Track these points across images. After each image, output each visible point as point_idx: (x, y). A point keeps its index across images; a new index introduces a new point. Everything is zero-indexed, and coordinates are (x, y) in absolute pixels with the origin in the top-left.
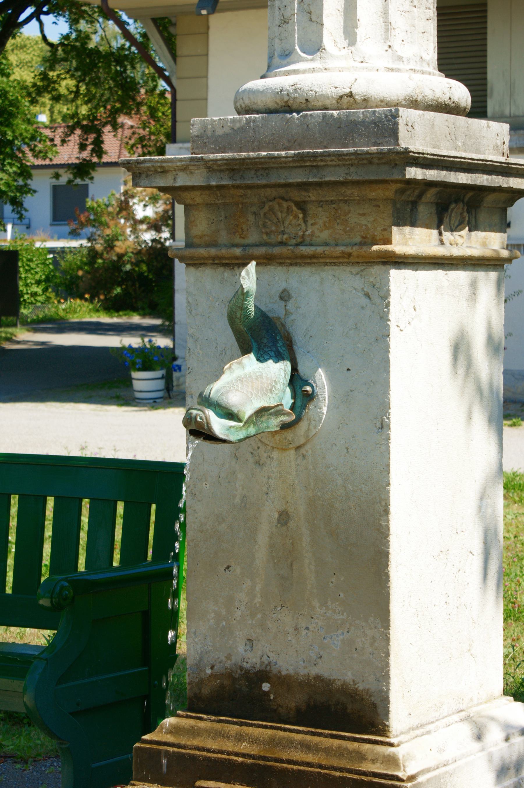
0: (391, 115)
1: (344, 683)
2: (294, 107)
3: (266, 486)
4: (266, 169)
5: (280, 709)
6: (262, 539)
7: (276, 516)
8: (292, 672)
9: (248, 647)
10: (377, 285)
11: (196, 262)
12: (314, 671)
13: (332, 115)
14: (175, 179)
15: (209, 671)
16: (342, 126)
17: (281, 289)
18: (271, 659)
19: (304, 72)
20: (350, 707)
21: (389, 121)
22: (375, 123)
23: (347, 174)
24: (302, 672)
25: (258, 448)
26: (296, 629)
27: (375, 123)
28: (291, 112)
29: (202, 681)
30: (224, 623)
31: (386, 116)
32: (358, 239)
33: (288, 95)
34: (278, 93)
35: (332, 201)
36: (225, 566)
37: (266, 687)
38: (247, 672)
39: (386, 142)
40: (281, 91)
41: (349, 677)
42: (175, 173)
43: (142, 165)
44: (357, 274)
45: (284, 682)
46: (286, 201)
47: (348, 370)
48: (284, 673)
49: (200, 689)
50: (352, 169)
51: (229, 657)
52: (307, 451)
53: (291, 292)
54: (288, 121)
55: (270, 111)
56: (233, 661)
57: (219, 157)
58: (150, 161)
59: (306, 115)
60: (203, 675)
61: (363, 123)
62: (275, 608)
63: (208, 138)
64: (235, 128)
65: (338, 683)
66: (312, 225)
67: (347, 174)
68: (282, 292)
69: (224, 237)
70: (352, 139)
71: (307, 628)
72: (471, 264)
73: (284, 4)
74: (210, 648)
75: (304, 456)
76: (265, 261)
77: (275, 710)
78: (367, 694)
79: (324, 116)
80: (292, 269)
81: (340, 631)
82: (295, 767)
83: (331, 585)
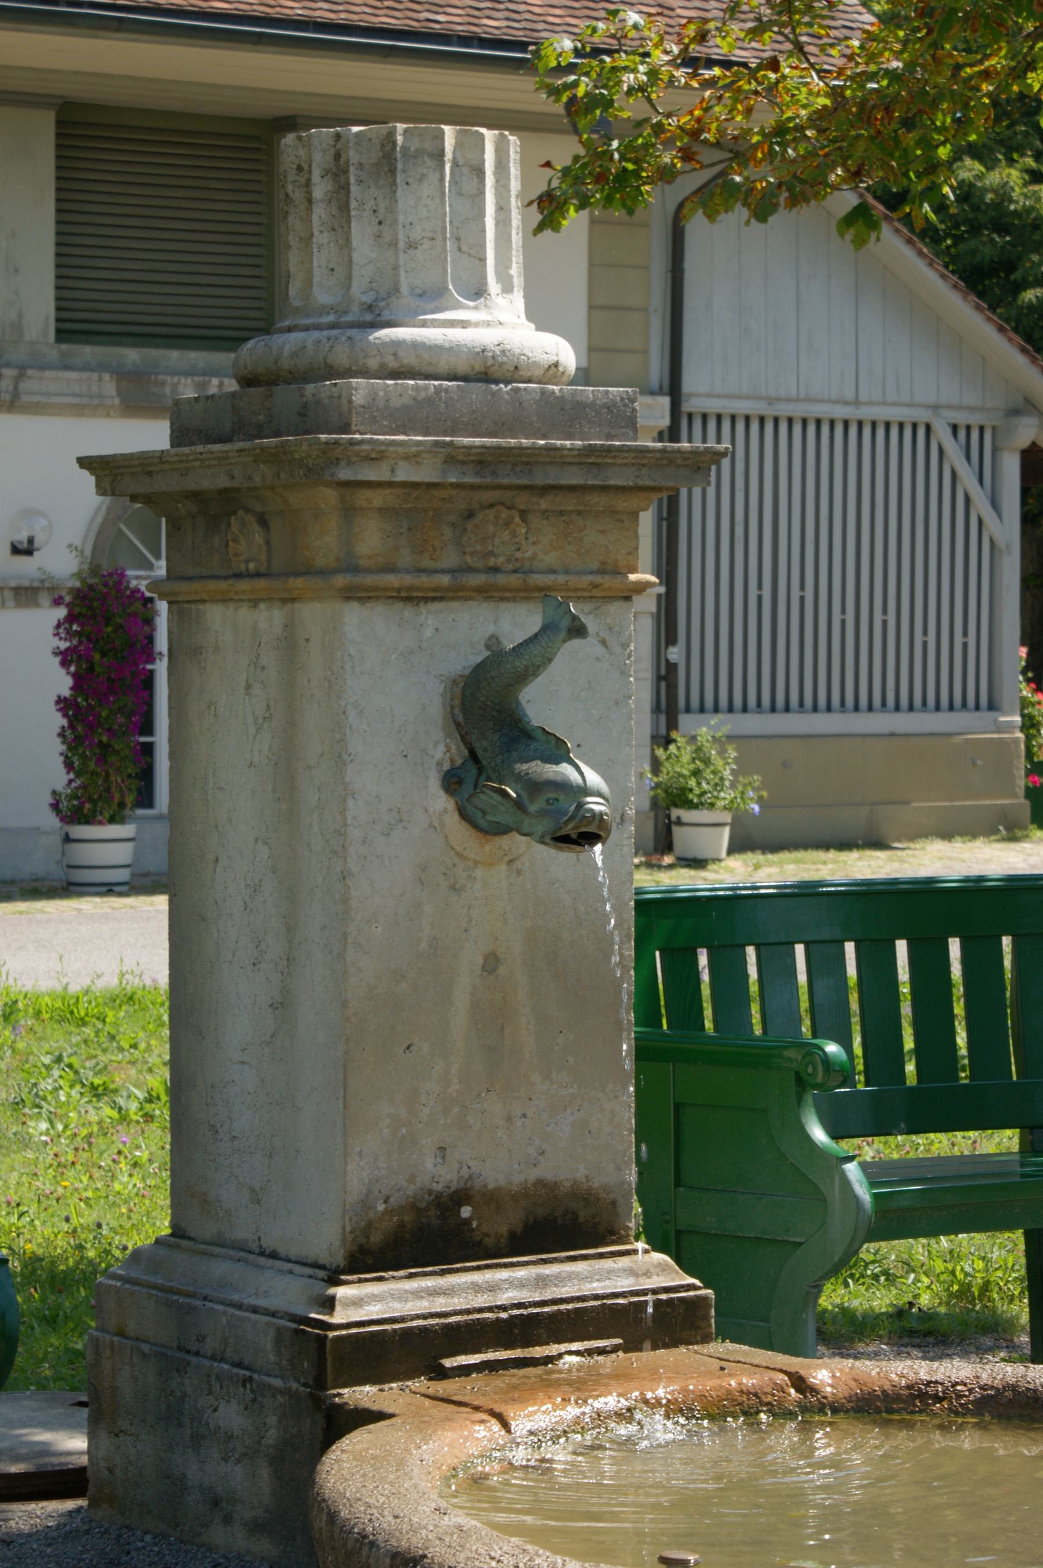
0: (628, 399)
1: (575, 1182)
2: (497, 375)
3: (466, 919)
4: (528, 463)
5: (486, 1239)
6: (461, 998)
7: (480, 961)
8: (502, 1182)
9: (439, 1160)
10: (616, 629)
11: (371, 594)
12: (533, 1175)
13: (553, 392)
14: (393, 471)
15: (381, 1207)
16: (567, 407)
17: (488, 635)
18: (473, 1169)
19: (477, 325)
20: (581, 1214)
21: (626, 406)
22: (608, 408)
23: (637, 477)
24: (517, 1179)
25: (454, 865)
26: (509, 1119)
27: (608, 408)
28: (497, 382)
29: (370, 1224)
30: (404, 1131)
31: (622, 399)
32: (595, 566)
33: (493, 357)
34: (478, 353)
35: (561, 512)
36: (406, 1045)
37: (466, 1212)
38: (439, 1196)
39: (623, 434)
40: (483, 351)
41: (580, 1173)
42: (392, 462)
43: (357, 448)
44: (590, 613)
45: (492, 1199)
46: (509, 508)
47: (579, 745)
48: (491, 1187)
49: (368, 1238)
50: (644, 471)
51: (412, 1180)
52: (523, 864)
53: (501, 639)
54: (493, 394)
55: (465, 379)
56: (418, 1185)
57: (477, 444)
58: (371, 441)
59: (519, 389)
60: (371, 1215)
61: (592, 405)
62: (479, 1094)
63: (378, 410)
64: (419, 399)
65: (567, 1184)
66: (533, 543)
67: (637, 477)
68: (489, 639)
69: (405, 558)
70: (580, 428)
71: (524, 1116)
72: (280, 599)
73: (410, 220)
74: (384, 1172)
75: (519, 872)
76: (475, 594)
77: (480, 1242)
78: (604, 1190)
79: (543, 392)
80: (503, 605)
81: (568, 1111)
82: (570, 1306)
83: (556, 1048)
